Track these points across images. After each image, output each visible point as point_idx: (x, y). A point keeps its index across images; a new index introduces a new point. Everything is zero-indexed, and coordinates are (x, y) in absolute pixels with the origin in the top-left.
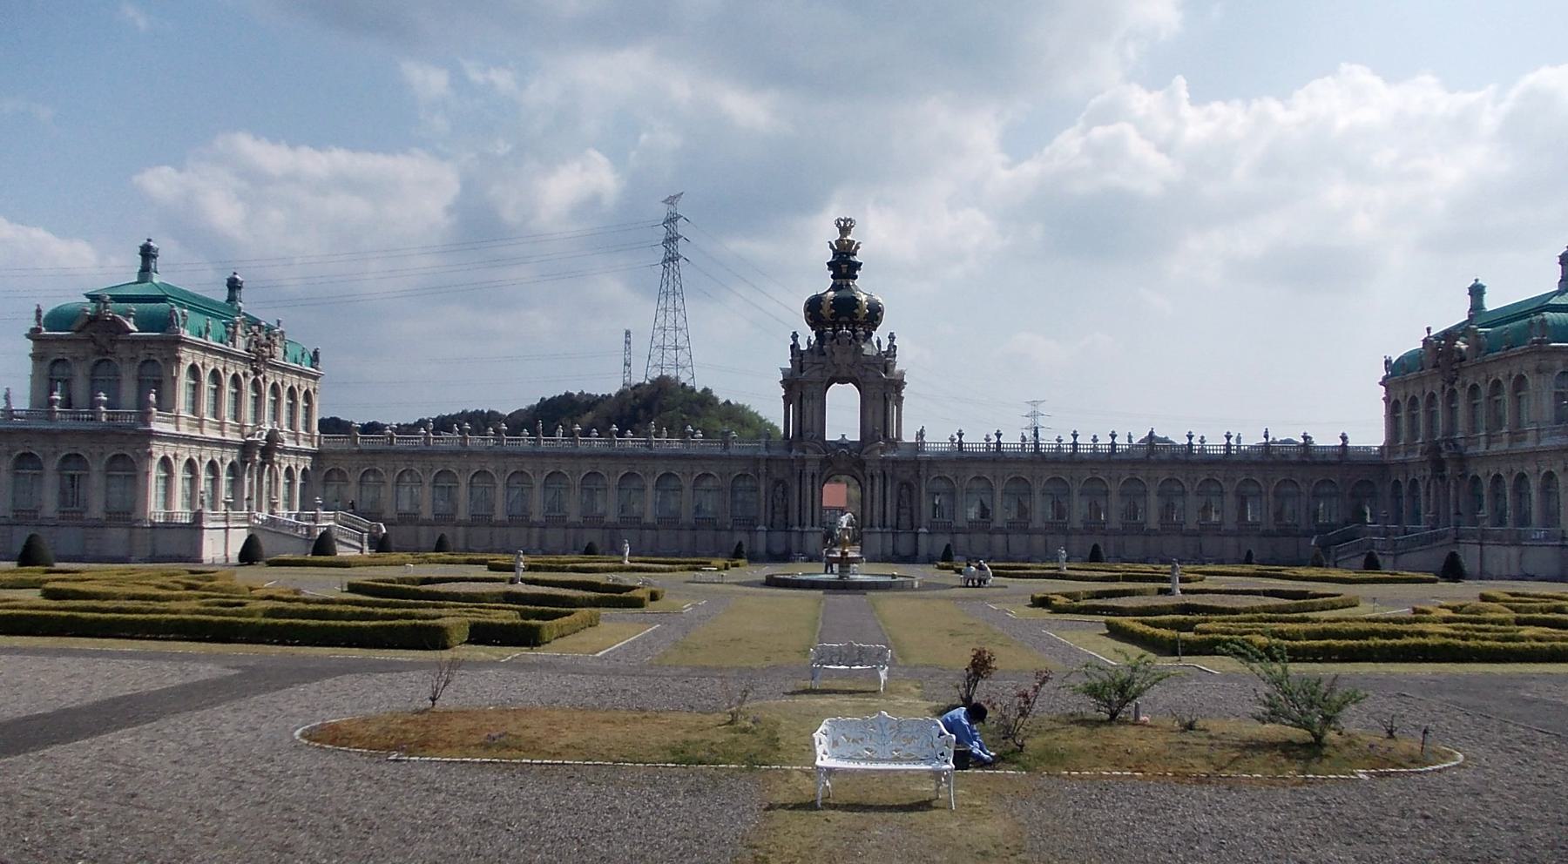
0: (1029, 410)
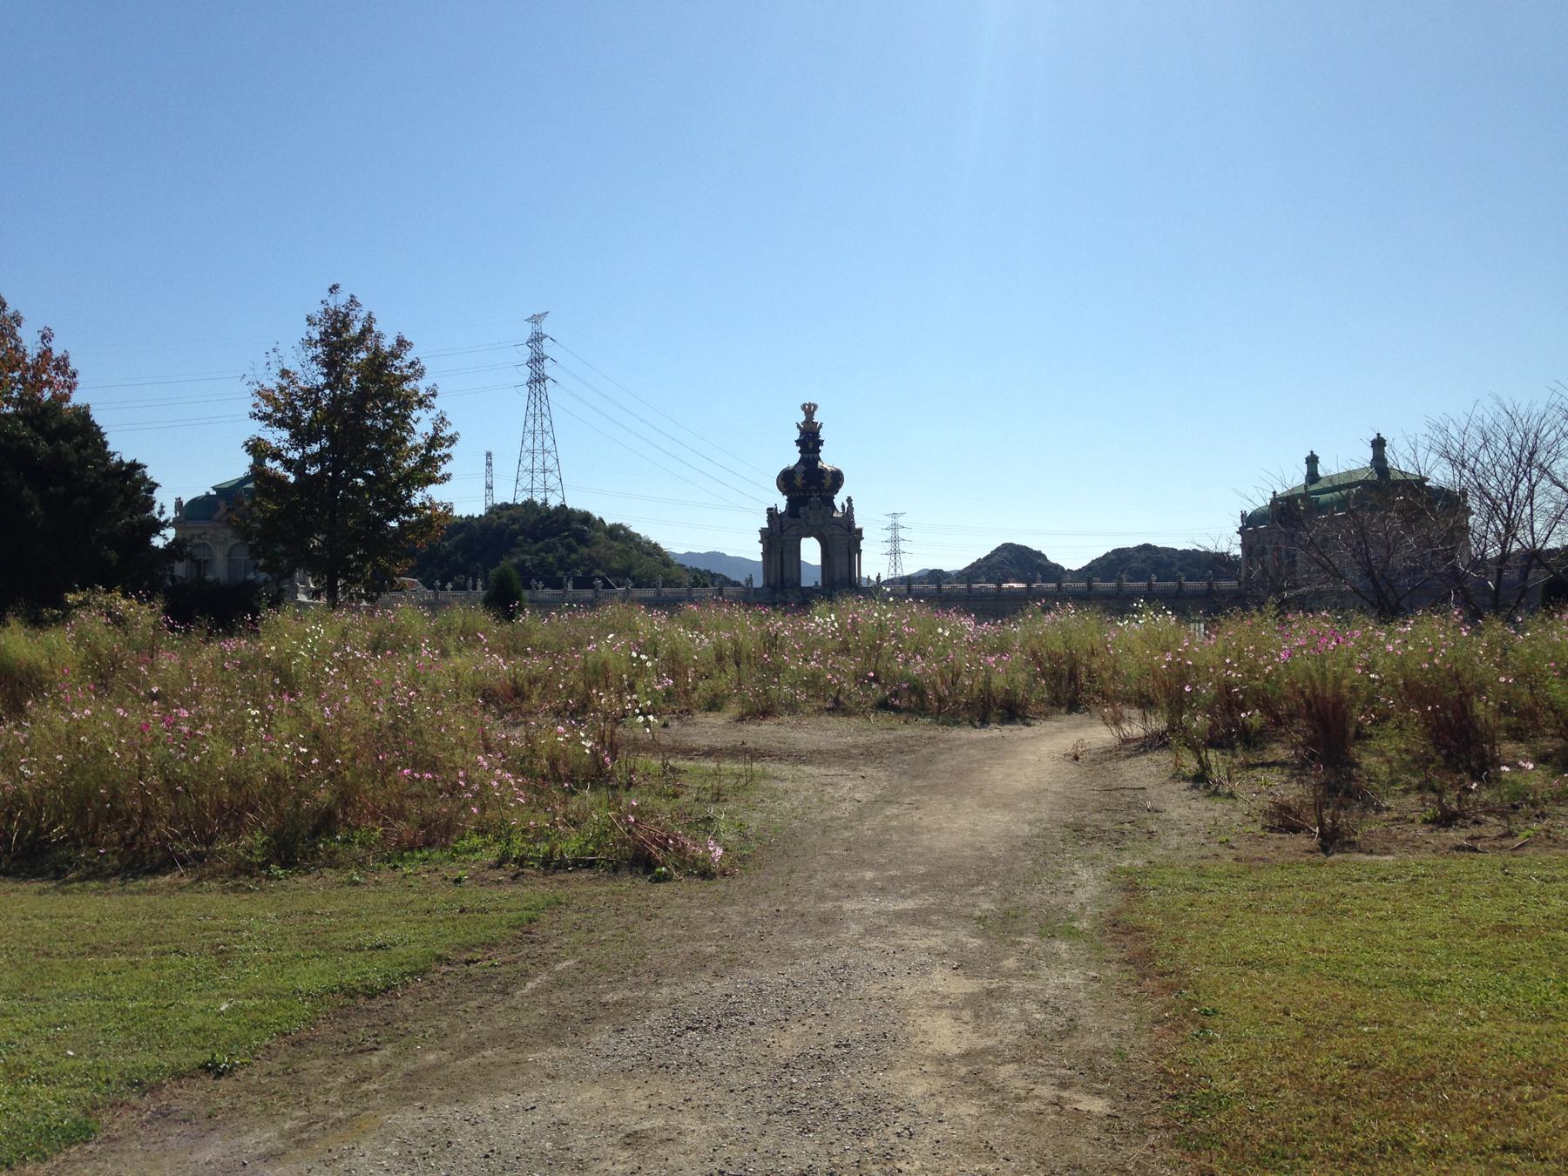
0: (889, 521)
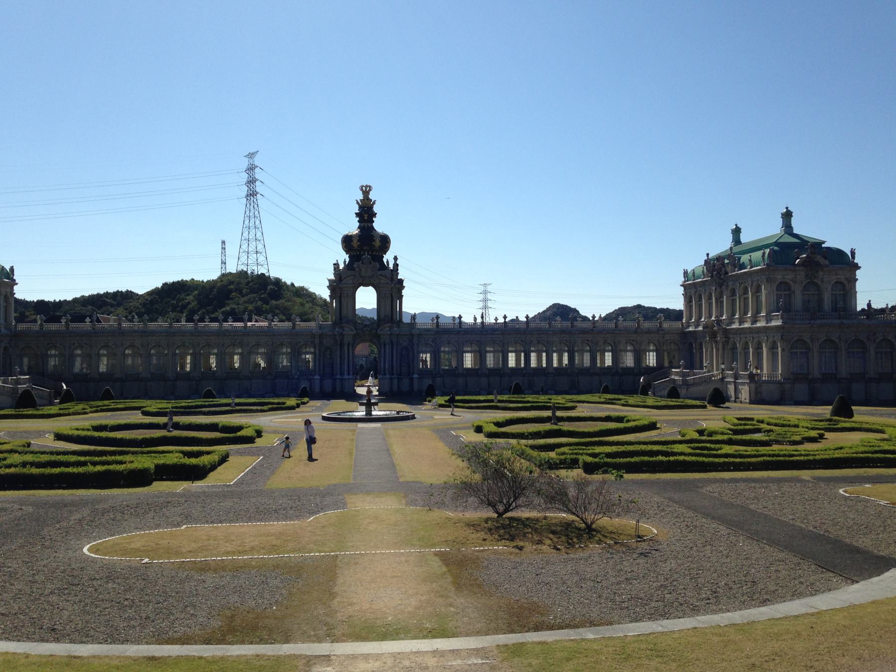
0: (482, 288)
